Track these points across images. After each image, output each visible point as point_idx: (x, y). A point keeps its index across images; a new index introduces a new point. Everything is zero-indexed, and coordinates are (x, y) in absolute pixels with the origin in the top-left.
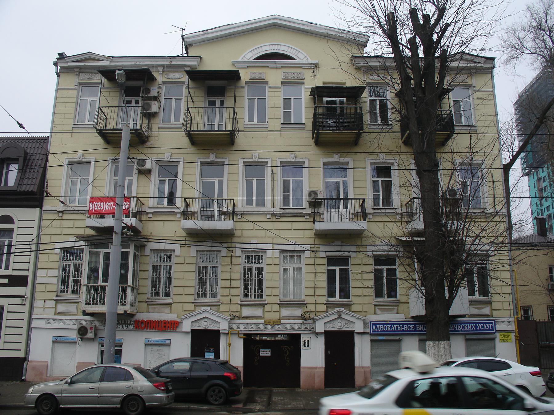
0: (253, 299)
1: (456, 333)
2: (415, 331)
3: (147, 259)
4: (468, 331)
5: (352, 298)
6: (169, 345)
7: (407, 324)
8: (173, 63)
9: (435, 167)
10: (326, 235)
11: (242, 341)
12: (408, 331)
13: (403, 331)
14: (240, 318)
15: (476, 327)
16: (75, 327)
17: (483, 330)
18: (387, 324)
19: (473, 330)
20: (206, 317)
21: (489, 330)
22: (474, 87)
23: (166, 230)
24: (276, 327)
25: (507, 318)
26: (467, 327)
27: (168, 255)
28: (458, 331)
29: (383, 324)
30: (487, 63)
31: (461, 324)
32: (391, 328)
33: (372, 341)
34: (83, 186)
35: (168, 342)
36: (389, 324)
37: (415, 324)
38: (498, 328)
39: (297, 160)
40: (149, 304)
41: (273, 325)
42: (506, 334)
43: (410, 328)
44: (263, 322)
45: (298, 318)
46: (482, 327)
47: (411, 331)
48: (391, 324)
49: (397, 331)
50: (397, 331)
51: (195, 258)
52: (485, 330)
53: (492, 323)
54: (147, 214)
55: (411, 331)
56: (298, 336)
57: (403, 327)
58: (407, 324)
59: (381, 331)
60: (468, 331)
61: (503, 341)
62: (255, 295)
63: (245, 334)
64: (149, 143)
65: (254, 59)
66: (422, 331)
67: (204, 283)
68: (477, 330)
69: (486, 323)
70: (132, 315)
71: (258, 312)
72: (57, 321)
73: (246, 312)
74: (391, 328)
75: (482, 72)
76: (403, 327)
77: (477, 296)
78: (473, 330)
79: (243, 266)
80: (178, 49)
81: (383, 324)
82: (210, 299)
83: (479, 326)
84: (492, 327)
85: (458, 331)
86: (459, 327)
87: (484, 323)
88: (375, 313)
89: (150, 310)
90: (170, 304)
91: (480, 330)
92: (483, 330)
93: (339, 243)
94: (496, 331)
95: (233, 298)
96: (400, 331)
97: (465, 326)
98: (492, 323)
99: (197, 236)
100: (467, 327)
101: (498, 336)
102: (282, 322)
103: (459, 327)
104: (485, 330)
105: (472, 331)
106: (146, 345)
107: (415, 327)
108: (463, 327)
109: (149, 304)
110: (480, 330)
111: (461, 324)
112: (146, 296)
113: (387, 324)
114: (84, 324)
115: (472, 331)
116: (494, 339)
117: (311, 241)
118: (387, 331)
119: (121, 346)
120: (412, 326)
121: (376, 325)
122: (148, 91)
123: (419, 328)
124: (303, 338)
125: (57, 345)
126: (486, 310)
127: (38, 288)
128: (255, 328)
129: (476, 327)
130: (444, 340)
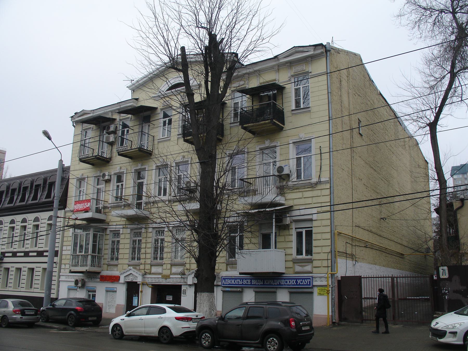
0: (159, 261)
1: (280, 287)
2: (251, 284)
3: (108, 237)
4: (290, 285)
5: (315, 256)
6: (116, 291)
7: (246, 279)
8: (122, 106)
9: (213, 158)
10: (131, 219)
11: (151, 289)
12: (246, 284)
13: (243, 284)
14: (150, 273)
15: (296, 282)
16: (74, 280)
17: (302, 285)
18: (232, 279)
19: (294, 285)
20: (131, 274)
21: (307, 285)
22: (311, 73)
23: (115, 218)
24: (168, 280)
25: (323, 275)
26: (290, 282)
27: (116, 234)
28: (282, 285)
29: (230, 279)
30: (318, 49)
31: (285, 279)
32: (234, 282)
33: (224, 292)
34: (84, 192)
35: (115, 289)
36: (233, 279)
37: (251, 279)
38: (315, 283)
39: (184, 160)
40: (109, 265)
41: (166, 279)
42: (323, 288)
43: (247, 282)
44: (160, 276)
45: (179, 274)
46: (301, 282)
47: (248, 285)
48: (235, 279)
49: (239, 284)
50: (239, 284)
51: (129, 235)
52: (304, 285)
53: (310, 279)
54: (108, 208)
55: (248, 285)
56: (179, 287)
57: (243, 281)
58: (246, 279)
59: (228, 284)
60: (290, 285)
61: (320, 294)
62: (160, 258)
63: (152, 285)
64: (153, 154)
65: (167, 91)
66: (256, 285)
67: (136, 250)
68: (297, 285)
69: (304, 279)
70: (99, 273)
71: (159, 270)
72: (70, 277)
73: (154, 270)
74: (234, 282)
75: (315, 58)
76: (243, 281)
77: (304, 256)
78: (294, 285)
79: (154, 238)
80: (127, 95)
81: (230, 279)
82: (138, 261)
83: (299, 281)
84: (310, 282)
85: (282, 285)
86: (283, 282)
87: (303, 279)
88: (227, 270)
89: (109, 269)
90: (117, 265)
91: (299, 285)
92: (302, 285)
93: (137, 223)
94: (314, 286)
95: (146, 260)
96: (241, 285)
97: (288, 281)
98: (310, 279)
99: (131, 219)
100: (290, 282)
101: (316, 290)
102: (171, 276)
103: (283, 282)
104: (304, 285)
105: (293, 285)
106: (107, 291)
107: (251, 282)
108: (286, 282)
109: (109, 265)
110: (299, 285)
111: (285, 279)
112: (107, 260)
113: (232, 279)
114: (77, 278)
115: (293, 285)
116: (312, 293)
117: (124, 223)
118: (232, 284)
119: (95, 292)
120: (249, 281)
121: (225, 279)
122: (109, 128)
123: (254, 282)
124: (183, 288)
125: (71, 291)
126: (308, 268)
127: (64, 257)
128: (157, 280)
129: (296, 282)
130: (204, 292)
